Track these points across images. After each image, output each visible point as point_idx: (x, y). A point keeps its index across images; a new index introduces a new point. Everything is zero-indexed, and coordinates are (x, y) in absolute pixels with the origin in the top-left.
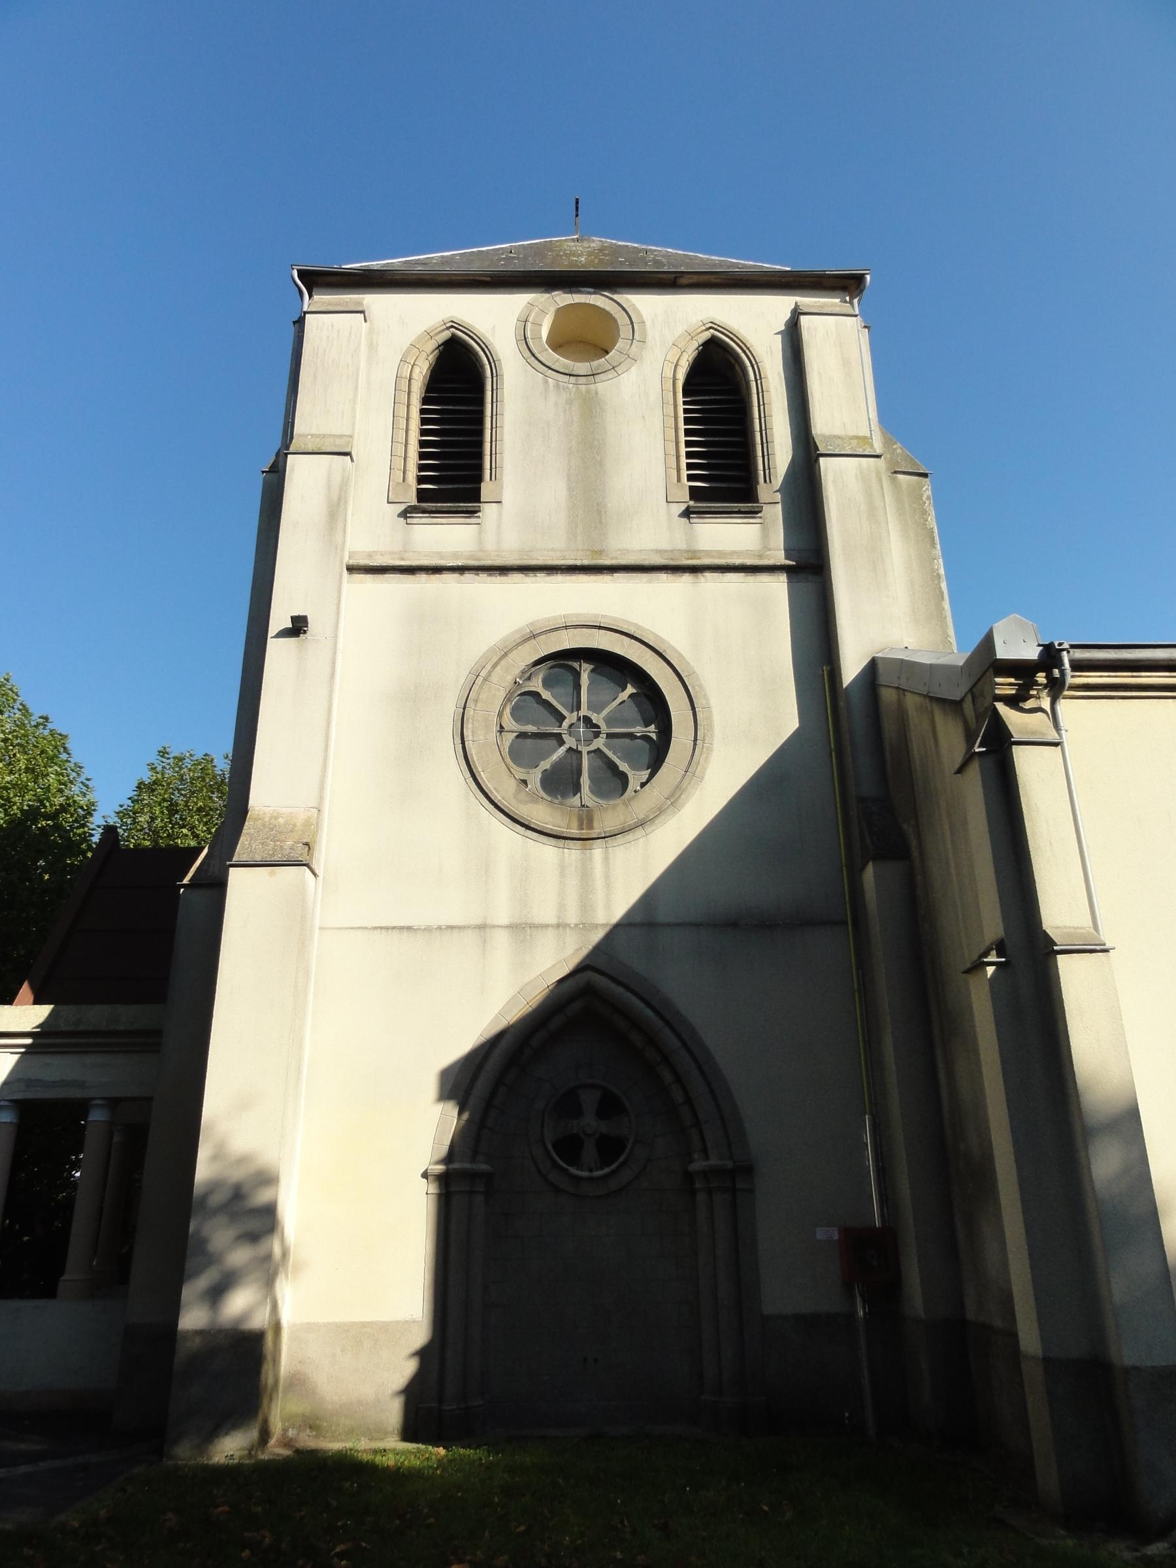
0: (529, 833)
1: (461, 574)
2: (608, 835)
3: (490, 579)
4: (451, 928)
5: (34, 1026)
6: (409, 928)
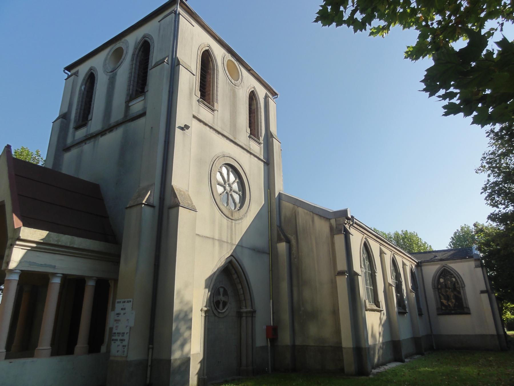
0: (222, 214)
3: (215, 133)
4: (207, 237)
5: (40, 239)
6: (199, 235)
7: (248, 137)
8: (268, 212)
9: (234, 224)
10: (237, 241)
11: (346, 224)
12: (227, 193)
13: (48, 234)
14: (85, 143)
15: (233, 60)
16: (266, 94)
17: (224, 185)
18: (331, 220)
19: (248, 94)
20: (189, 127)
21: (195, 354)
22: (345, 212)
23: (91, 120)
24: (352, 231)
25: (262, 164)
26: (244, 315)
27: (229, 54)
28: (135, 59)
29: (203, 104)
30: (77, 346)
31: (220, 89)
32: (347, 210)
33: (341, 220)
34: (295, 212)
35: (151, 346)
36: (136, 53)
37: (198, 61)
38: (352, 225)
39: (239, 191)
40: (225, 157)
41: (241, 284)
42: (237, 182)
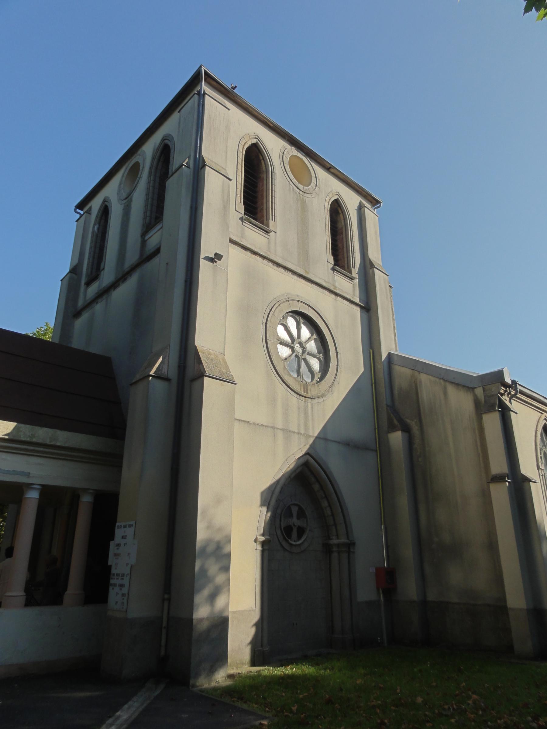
0: (288, 389)
1: (263, 259)
2: (313, 397)
4: (262, 425)
5: (4, 434)
6: (248, 422)
7: (331, 269)
8: (372, 385)
9: (309, 404)
10: (316, 430)
11: (502, 395)
12: (296, 356)
13: (16, 426)
14: (97, 303)
15: (300, 155)
16: (360, 203)
17: (292, 345)
18: (475, 390)
19: (328, 204)
20: (222, 256)
21: (246, 611)
22: (499, 375)
23: (103, 269)
24: (514, 405)
25: (357, 310)
26: (335, 549)
27: (293, 147)
28: (152, 174)
29: (249, 222)
30: (67, 592)
31: (277, 200)
32: (503, 370)
33: (493, 388)
34: (414, 382)
35: (166, 596)
36: (155, 165)
37: (240, 161)
38: (515, 395)
39: (319, 353)
40: (291, 302)
41: (327, 500)
42: (315, 339)
